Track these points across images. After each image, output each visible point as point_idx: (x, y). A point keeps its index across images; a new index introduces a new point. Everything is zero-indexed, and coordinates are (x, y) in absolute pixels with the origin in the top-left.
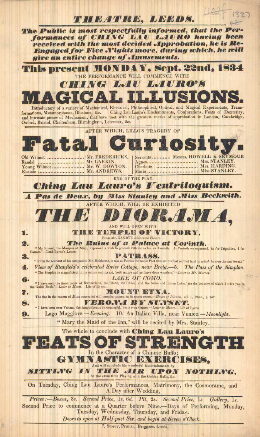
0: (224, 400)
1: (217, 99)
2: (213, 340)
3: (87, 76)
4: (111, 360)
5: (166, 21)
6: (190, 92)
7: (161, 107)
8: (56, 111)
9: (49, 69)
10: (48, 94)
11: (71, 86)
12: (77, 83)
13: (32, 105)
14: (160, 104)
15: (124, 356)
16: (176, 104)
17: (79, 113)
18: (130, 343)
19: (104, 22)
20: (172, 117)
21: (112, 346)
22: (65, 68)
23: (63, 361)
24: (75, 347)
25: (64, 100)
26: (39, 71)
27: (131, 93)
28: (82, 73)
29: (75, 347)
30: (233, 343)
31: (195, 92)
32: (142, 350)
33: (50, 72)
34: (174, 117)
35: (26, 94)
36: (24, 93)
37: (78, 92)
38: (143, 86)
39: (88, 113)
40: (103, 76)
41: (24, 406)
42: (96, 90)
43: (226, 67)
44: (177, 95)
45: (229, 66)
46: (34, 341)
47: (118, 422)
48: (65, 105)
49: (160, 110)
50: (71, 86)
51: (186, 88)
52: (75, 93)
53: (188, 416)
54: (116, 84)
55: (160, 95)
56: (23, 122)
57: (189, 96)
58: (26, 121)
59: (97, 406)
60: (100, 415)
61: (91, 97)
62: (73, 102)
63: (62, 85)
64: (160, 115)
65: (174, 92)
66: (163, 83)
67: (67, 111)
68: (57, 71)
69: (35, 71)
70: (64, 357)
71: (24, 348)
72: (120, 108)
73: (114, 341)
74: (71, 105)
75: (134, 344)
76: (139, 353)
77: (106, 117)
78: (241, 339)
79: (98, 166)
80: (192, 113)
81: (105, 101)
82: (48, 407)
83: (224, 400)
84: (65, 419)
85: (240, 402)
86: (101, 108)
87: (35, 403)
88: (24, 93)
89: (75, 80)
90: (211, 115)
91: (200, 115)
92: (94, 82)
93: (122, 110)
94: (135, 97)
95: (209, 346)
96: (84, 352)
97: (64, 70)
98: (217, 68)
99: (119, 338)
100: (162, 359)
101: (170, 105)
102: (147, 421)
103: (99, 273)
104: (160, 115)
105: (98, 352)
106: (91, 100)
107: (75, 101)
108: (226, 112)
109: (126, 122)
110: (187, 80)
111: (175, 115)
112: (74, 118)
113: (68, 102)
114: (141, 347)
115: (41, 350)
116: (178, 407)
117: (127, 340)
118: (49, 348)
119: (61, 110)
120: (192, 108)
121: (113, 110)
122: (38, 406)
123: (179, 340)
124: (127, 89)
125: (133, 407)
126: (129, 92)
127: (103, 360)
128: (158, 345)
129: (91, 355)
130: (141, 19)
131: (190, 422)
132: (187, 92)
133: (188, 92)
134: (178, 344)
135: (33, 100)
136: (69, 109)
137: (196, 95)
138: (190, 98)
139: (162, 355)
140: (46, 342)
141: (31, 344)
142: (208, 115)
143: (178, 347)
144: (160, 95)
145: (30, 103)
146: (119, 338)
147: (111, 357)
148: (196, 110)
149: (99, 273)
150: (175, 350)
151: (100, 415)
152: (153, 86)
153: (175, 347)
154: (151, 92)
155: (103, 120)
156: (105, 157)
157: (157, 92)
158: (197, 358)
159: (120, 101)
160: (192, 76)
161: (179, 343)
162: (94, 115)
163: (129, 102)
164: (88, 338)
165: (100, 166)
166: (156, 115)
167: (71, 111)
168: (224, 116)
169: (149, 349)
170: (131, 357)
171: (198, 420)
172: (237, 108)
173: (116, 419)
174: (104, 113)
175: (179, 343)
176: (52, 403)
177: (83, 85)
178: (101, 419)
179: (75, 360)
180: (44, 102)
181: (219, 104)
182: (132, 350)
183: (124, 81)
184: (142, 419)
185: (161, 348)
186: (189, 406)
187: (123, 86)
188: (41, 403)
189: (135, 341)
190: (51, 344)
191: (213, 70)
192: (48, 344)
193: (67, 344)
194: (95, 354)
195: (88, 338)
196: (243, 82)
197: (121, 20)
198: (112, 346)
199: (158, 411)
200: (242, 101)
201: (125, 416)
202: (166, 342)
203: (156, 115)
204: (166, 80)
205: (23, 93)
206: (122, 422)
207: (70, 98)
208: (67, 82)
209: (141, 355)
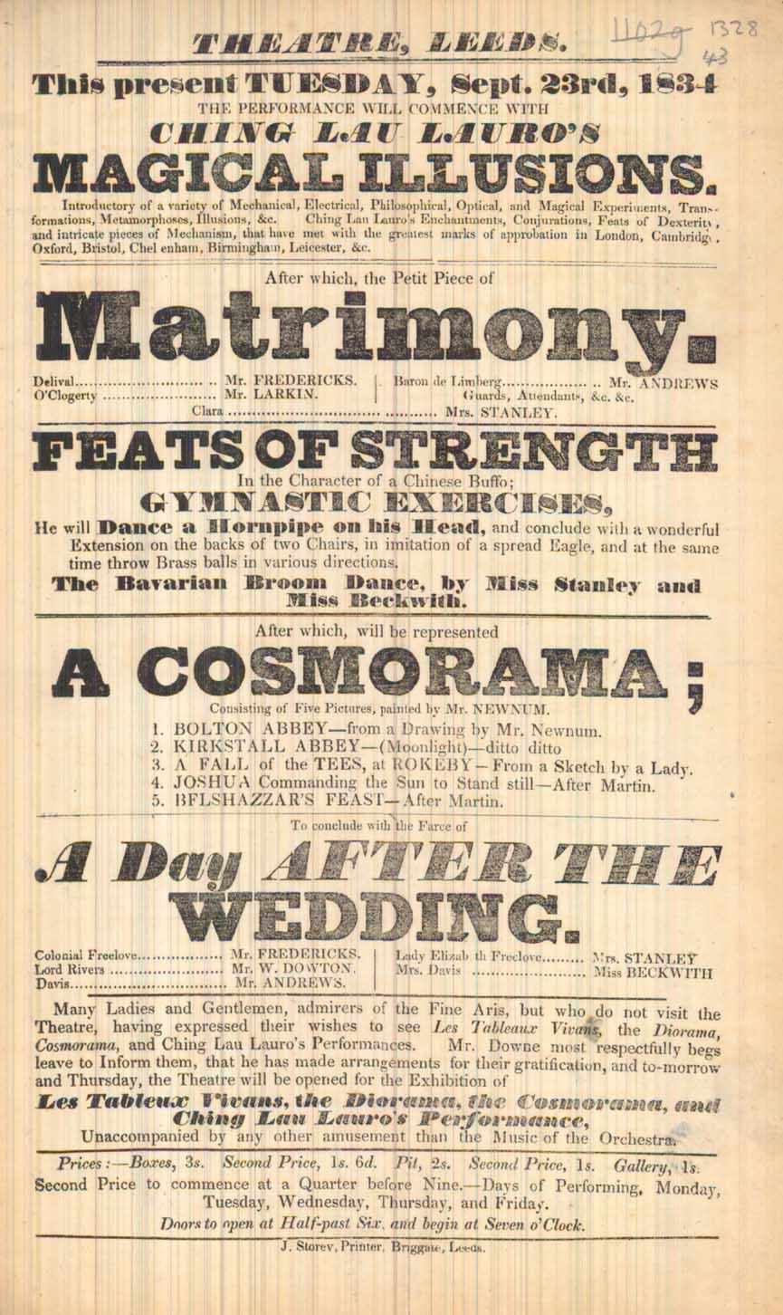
0: (657, 1169)
1: (635, 179)
2: (622, 444)
3: (234, 108)
4: (308, 503)
5: (472, 875)
6: (553, 158)
7: (461, 204)
8: (138, 213)
9: (113, 83)
10: (113, 162)
11: (184, 139)
12: (202, 128)
13: (64, 195)
14: (459, 196)
15: (347, 492)
16: (508, 195)
17: (207, 219)
19: (288, 51)
20: (497, 235)
21: (309, 462)
22: (165, 83)
23: (159, 507)
24: (197, 465)
25: (164, 179)
26: (84, 90)
27: (371, 161)
28: (215, 98)
29: (197, 465)
30: (683, 452)
31: (569, 158)
32: (402, 473)
33: (119, 96)
34: (503, 235)
35: (45, 160)
37: (206, 156)
38: (406, 138)
39: (238, 220)
40: (283, 108)
41: (40, 1185)
42: (262, 150)
43: (663, 83)
44: (511, 166)
45: (675, 80)
46: (69, 446)
47: (330, 1232)
48: (165, 197)
49: (459, 214)
50: (184, 139)
51: (540, 147)
52: (197, 160)
53: (545, 1215)
54: (325, 132)
55: (460, 166)
56: (37, 248)
57: (549, 170)
58: (46, 243)
59: (265, 1185)
60: (277, 1212)
61: (247, 172)
62: (190, 187)
63: (156, 133)
64: (458, 228)
65: (503, 160)
66: (469, 128)
67: (175, 214)
68: (140, 91)
69: (73, 91)
70: (162, 496)
71: (37, 467)
72: (337, 206)
73: (315, 444)
74: (183, 195)
75: (379, 455)
76: (393, 483)
77: (291, 234)
78: (708, 440)
79: (265, 968)
80: (557, 222)
81: (289, 184)
82: (114, 1186)
83: (657, 1169)
84: (167, 1225)
85: (707, 1173)
86: (277, 207)
87: (72, 1175)
89: (197, 119)
90: (617, 230)
91: (584, 228)
92: (256, 127)
93: (343, 213)
94: (384, 173)
95: (610, 462)
96: (224, 481)
97: (163, 89)
98: (635, 85)
99: (333, 438)
100: (464, 502)
101: (487, 198)
102: (418, 1231)
104: (458, 228)
105: (266, 480)
106: (245, 181)
107: (197, 185)
108: (664, 221)
109: (356, 249)
110: (542, 121)
111: (505, 230)
112: (194, 234)
113: (175, 189)
114: (397, 464)
115: (88, 473)
116: (516, 1187)
117: (356, 442)
118: (113, 468)
119: (153, 212)
120: (558, 208)
121: (315, 211)
122: (83, 1186)
124: (353, 149)
125: (377, 1186)
126: (362, 157)
127: (282, 503)
128: (451, 457)
129: (244, 489)
130: (402, 41)
131: (553, 1234)
132: (542, 158)
133: (548, 159)
134: (108, 455)
135: (68, 180)
136: (181, 207)
137: (571, 168)
138: (550, 177)
139: (465, 488)
140: (106, 451)
141: (58, 455)
142: (607, 229)
143: (513, 465)
144: (460, 166)
145: (59, 190)
146: (333, 438)
147: (307, 494)
148: (573, 215)
150: (505, 474)
151: (277, 1212)
152: (438, 141)
153: (504, 465)
154: (431, 158)
155: (284, 243)
156: (285, 379)
157: (450, 158)
158: (574, 499)
159: (338, 183)
160: (563, 108)
161: (517, 451)
162: (258, 227)
163: (363, 188)
164: (237, 436)
165: (273, 968)
166: (450, 228)
167: (184, 214)
168: (656, 236)
169: (424, 470)
170: (369, 494)
171: (576, 1228)
172: (697, 210)
173: (326, 1225)
174: (285, 220)
175: (517, 451)
176: (126, 1175)
177: (221, 137)
178: (277, 1223)
179: (196, 502)
180: (100, 186)
181: (643, 196)
182: (373, 473)
183: (346, 124)
184: (403, 1225)
185: (460, 466)
186: (550, 1185)
187: (344, 137)
188: (90, 1175)
189: (382, 446)
190: (121, 457)
191: (624, 90)
192: (112, 457)
194: (257, 486)
195: (237, 436)
196: (717, 282)
197: (339, 46)
198: (309, 462)
199: (454, 1198)
200: (712, 190)
201: (352, 1214)
202: (477, 450)
203: (450, 228)
204: (480, 121)
205: (37, 157)
206: (342, 1232)
207: (182, 173)
208: (171, 126)
209: (401, 488)
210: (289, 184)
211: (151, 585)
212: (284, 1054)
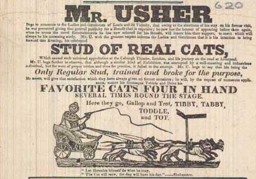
18: (219, 51)
21: (114, 53)
35: (70, 8)
36: (67, 7)
81: (161, 53)
88: (67, 7)
103: (33, 79)
106: (189, 52)
123: (188, 11)
128: (133, 52)
134: (186, 16)
149: (33, 79)
193: (205, 51)
198: (114, 53)
210: (161, 53)
211: (210, 105)
212: (190, 32)
